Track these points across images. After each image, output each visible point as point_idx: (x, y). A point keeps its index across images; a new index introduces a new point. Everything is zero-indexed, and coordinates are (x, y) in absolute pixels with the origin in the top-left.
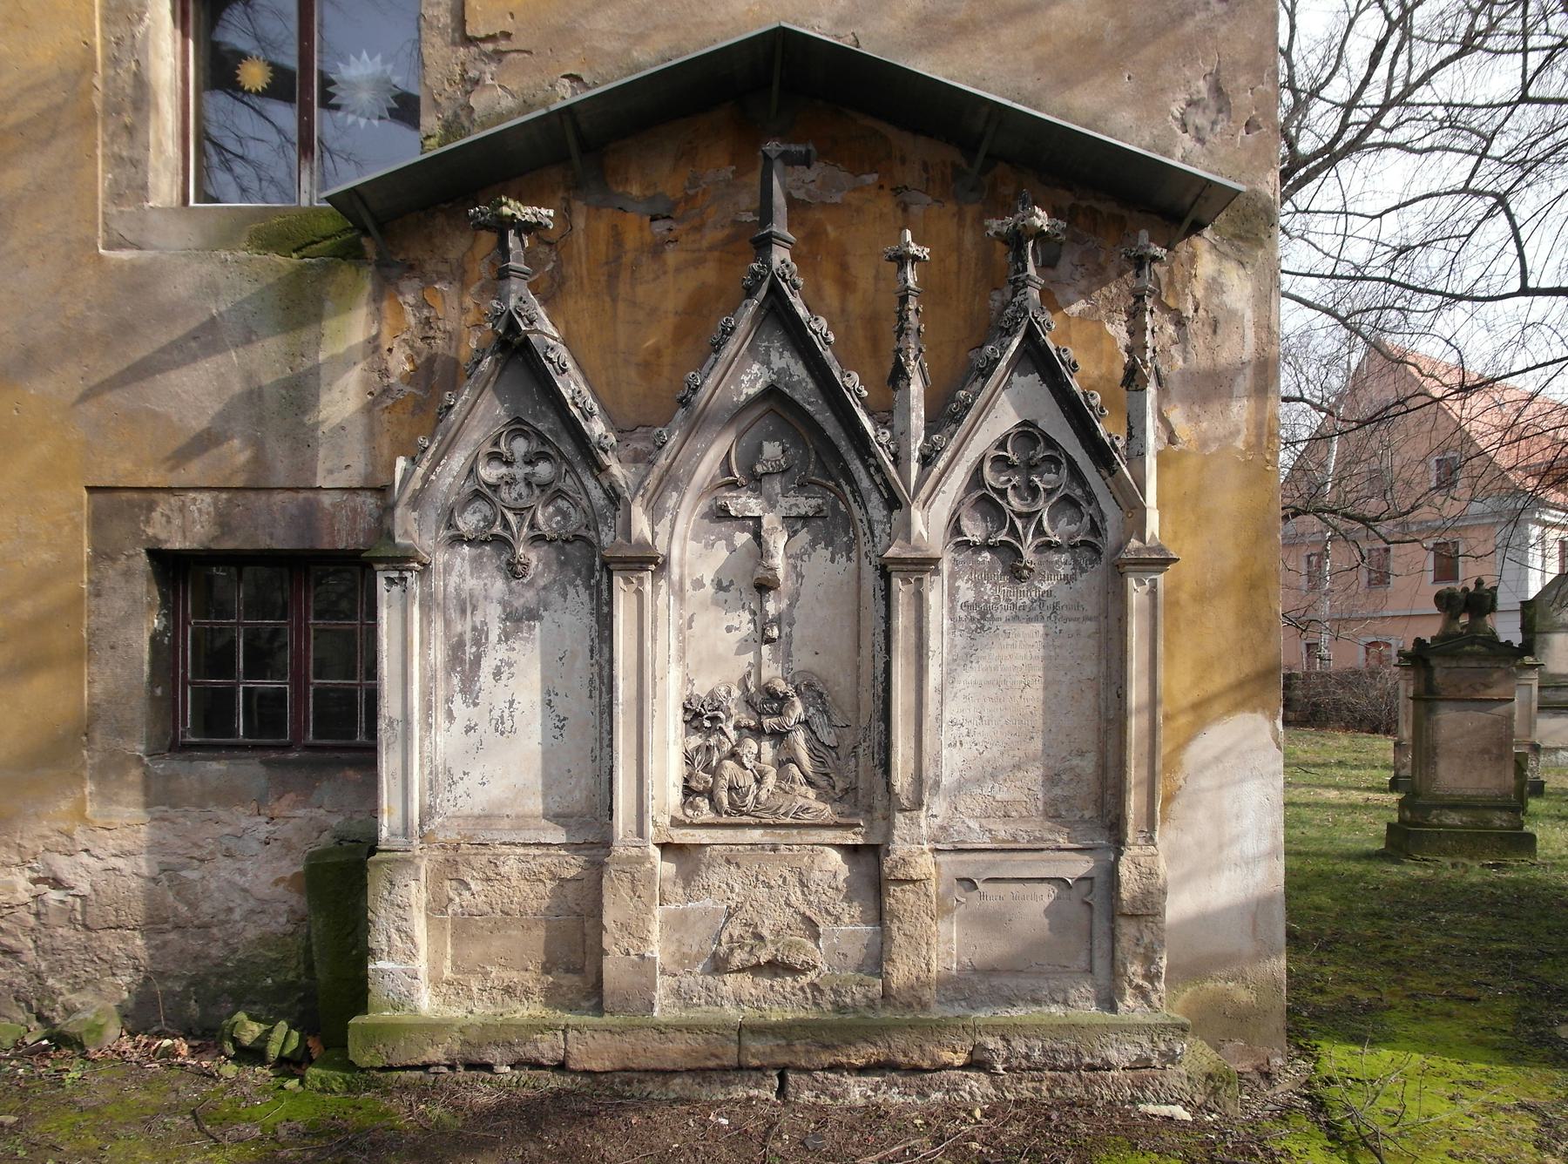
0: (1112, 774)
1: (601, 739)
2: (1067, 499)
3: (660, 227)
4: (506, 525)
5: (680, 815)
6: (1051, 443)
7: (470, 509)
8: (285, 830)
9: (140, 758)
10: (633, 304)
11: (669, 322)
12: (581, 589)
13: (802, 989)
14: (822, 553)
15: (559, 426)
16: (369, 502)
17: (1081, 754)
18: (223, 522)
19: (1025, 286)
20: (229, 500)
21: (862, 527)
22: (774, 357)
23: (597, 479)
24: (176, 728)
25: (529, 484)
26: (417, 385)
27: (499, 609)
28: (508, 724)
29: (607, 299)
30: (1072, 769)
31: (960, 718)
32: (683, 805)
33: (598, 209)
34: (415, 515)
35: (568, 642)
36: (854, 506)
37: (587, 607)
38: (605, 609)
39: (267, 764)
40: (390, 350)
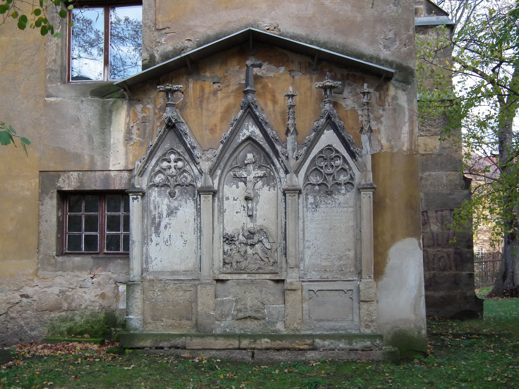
0: (359, 256)
1: (197, 247)
3: (216, 86)
6: (337, 152)
9: (54, 256)
10: (208, 110)
11: (219, 116)
12: (191, 201)
14: (266, 188)
15: (184, 150)
16: (126, 174)
17: (349, 250)
18: (80, 181)
20: (83, 175)
21: (278, 180)
22: (250, 127)
23: (196, 166)
24: (63, 248)
25: (175, 168)
26: (140, 137)
29: (200, 109)
30: (346, 255)
31: (309, 240)
33: (197, 81)
36: (276, 173)
37: (193, 206)
38: (199, 207)
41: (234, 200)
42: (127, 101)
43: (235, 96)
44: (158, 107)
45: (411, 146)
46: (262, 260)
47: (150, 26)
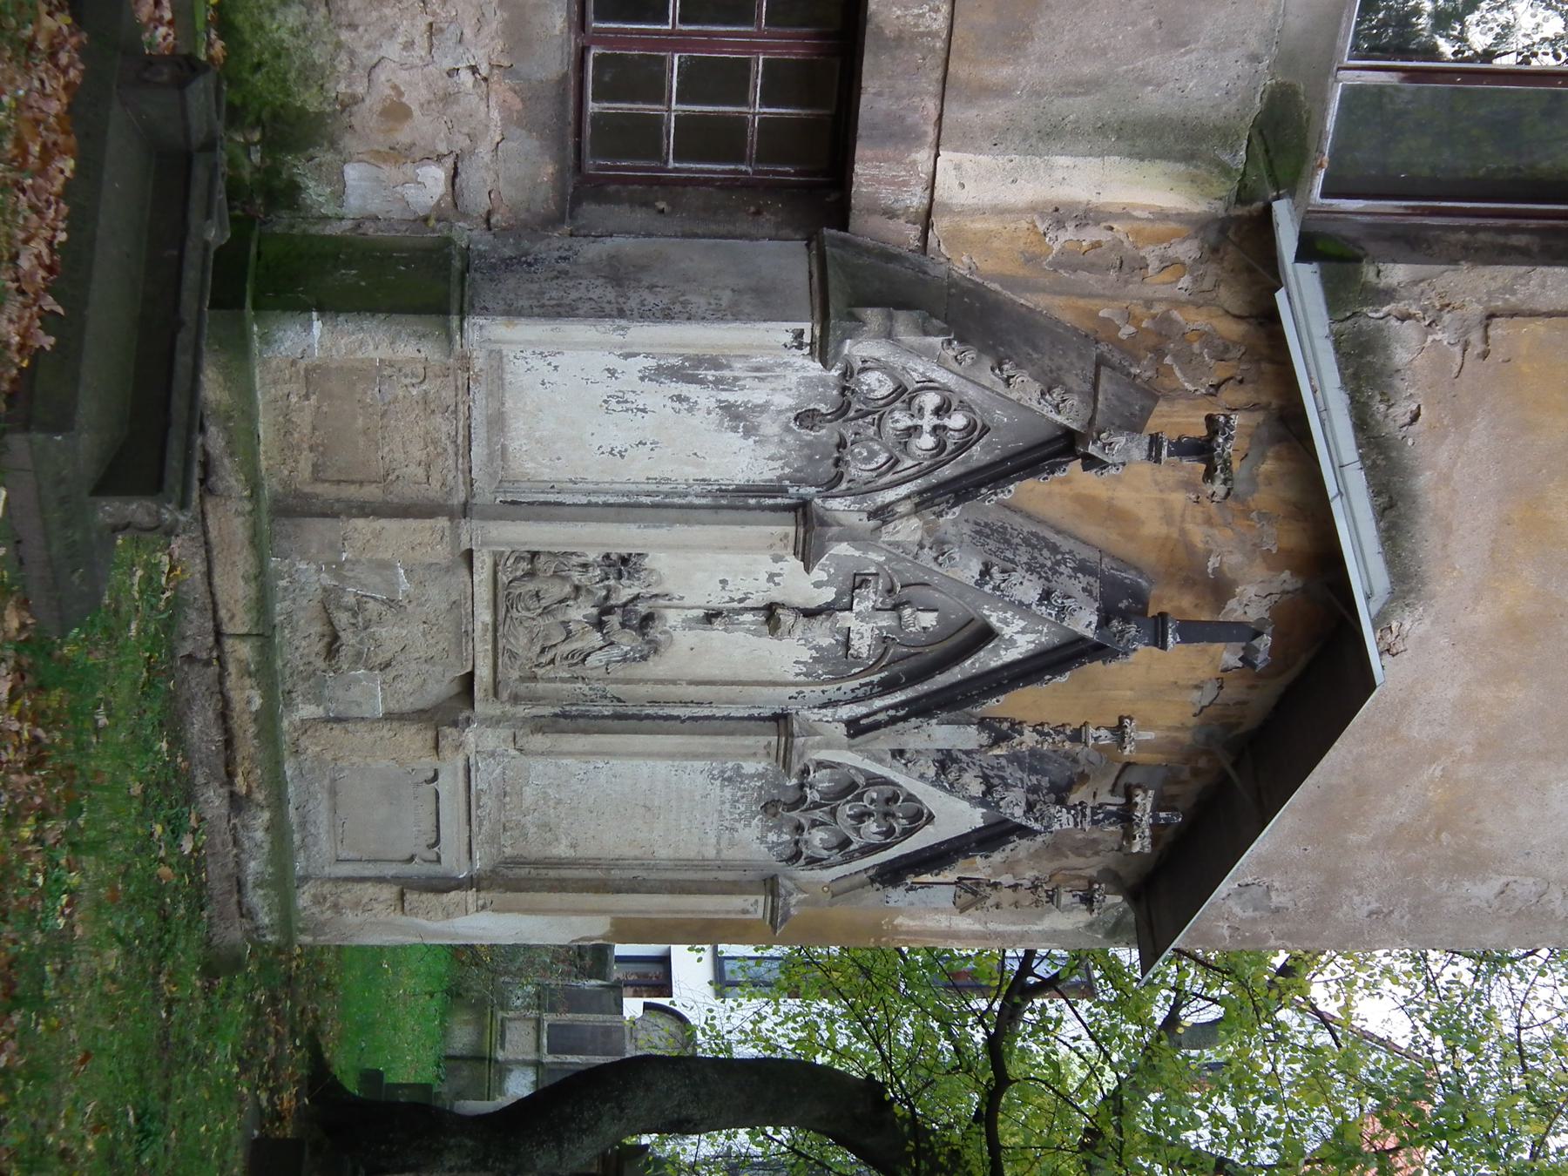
6: (907, 833)
12: (779, 472)
14: (806, 655)
16: (915, 199)
18: (904, 40)
20: (932, 50)
35: (714, 461)
41: (771, 577)
42: (1222, 213)
43: (1167, 538)
44: (1175, 314)
45: (908, 933)
46: (543, 651)
47: (1513, 292)
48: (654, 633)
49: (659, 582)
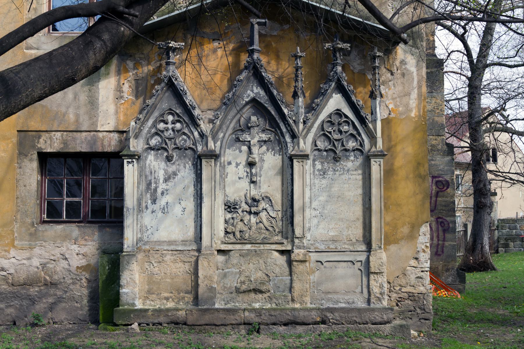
2: (352, 135)
4: (166, 144)
5: (224, 240)
6: (346, 116)
7: (154, 139)
8: (84, 250)
13: (265, 298)
18: (65, 143)
19: (337, 65)
20: (67, 135)
22: (255, 88)
23: (196, 129)
27: (163, 172)
28: (166, 210)
32: (225, 237)
34: (136, 140)
39: (78, 226)
40: (123, 84)
48: (257, 198)
49: (240, 197)
